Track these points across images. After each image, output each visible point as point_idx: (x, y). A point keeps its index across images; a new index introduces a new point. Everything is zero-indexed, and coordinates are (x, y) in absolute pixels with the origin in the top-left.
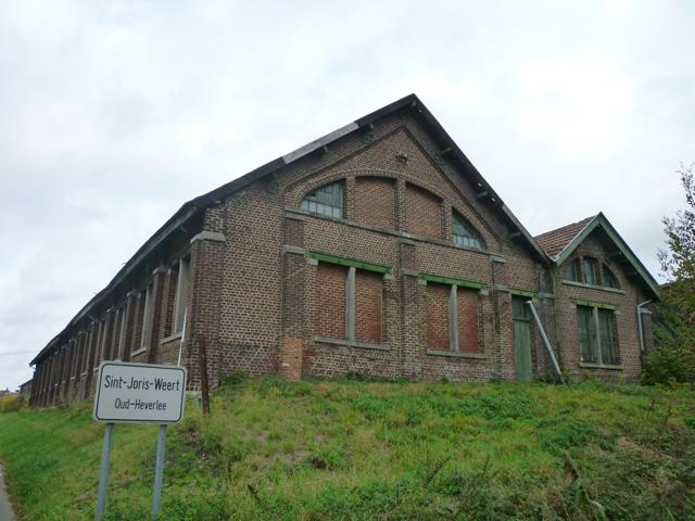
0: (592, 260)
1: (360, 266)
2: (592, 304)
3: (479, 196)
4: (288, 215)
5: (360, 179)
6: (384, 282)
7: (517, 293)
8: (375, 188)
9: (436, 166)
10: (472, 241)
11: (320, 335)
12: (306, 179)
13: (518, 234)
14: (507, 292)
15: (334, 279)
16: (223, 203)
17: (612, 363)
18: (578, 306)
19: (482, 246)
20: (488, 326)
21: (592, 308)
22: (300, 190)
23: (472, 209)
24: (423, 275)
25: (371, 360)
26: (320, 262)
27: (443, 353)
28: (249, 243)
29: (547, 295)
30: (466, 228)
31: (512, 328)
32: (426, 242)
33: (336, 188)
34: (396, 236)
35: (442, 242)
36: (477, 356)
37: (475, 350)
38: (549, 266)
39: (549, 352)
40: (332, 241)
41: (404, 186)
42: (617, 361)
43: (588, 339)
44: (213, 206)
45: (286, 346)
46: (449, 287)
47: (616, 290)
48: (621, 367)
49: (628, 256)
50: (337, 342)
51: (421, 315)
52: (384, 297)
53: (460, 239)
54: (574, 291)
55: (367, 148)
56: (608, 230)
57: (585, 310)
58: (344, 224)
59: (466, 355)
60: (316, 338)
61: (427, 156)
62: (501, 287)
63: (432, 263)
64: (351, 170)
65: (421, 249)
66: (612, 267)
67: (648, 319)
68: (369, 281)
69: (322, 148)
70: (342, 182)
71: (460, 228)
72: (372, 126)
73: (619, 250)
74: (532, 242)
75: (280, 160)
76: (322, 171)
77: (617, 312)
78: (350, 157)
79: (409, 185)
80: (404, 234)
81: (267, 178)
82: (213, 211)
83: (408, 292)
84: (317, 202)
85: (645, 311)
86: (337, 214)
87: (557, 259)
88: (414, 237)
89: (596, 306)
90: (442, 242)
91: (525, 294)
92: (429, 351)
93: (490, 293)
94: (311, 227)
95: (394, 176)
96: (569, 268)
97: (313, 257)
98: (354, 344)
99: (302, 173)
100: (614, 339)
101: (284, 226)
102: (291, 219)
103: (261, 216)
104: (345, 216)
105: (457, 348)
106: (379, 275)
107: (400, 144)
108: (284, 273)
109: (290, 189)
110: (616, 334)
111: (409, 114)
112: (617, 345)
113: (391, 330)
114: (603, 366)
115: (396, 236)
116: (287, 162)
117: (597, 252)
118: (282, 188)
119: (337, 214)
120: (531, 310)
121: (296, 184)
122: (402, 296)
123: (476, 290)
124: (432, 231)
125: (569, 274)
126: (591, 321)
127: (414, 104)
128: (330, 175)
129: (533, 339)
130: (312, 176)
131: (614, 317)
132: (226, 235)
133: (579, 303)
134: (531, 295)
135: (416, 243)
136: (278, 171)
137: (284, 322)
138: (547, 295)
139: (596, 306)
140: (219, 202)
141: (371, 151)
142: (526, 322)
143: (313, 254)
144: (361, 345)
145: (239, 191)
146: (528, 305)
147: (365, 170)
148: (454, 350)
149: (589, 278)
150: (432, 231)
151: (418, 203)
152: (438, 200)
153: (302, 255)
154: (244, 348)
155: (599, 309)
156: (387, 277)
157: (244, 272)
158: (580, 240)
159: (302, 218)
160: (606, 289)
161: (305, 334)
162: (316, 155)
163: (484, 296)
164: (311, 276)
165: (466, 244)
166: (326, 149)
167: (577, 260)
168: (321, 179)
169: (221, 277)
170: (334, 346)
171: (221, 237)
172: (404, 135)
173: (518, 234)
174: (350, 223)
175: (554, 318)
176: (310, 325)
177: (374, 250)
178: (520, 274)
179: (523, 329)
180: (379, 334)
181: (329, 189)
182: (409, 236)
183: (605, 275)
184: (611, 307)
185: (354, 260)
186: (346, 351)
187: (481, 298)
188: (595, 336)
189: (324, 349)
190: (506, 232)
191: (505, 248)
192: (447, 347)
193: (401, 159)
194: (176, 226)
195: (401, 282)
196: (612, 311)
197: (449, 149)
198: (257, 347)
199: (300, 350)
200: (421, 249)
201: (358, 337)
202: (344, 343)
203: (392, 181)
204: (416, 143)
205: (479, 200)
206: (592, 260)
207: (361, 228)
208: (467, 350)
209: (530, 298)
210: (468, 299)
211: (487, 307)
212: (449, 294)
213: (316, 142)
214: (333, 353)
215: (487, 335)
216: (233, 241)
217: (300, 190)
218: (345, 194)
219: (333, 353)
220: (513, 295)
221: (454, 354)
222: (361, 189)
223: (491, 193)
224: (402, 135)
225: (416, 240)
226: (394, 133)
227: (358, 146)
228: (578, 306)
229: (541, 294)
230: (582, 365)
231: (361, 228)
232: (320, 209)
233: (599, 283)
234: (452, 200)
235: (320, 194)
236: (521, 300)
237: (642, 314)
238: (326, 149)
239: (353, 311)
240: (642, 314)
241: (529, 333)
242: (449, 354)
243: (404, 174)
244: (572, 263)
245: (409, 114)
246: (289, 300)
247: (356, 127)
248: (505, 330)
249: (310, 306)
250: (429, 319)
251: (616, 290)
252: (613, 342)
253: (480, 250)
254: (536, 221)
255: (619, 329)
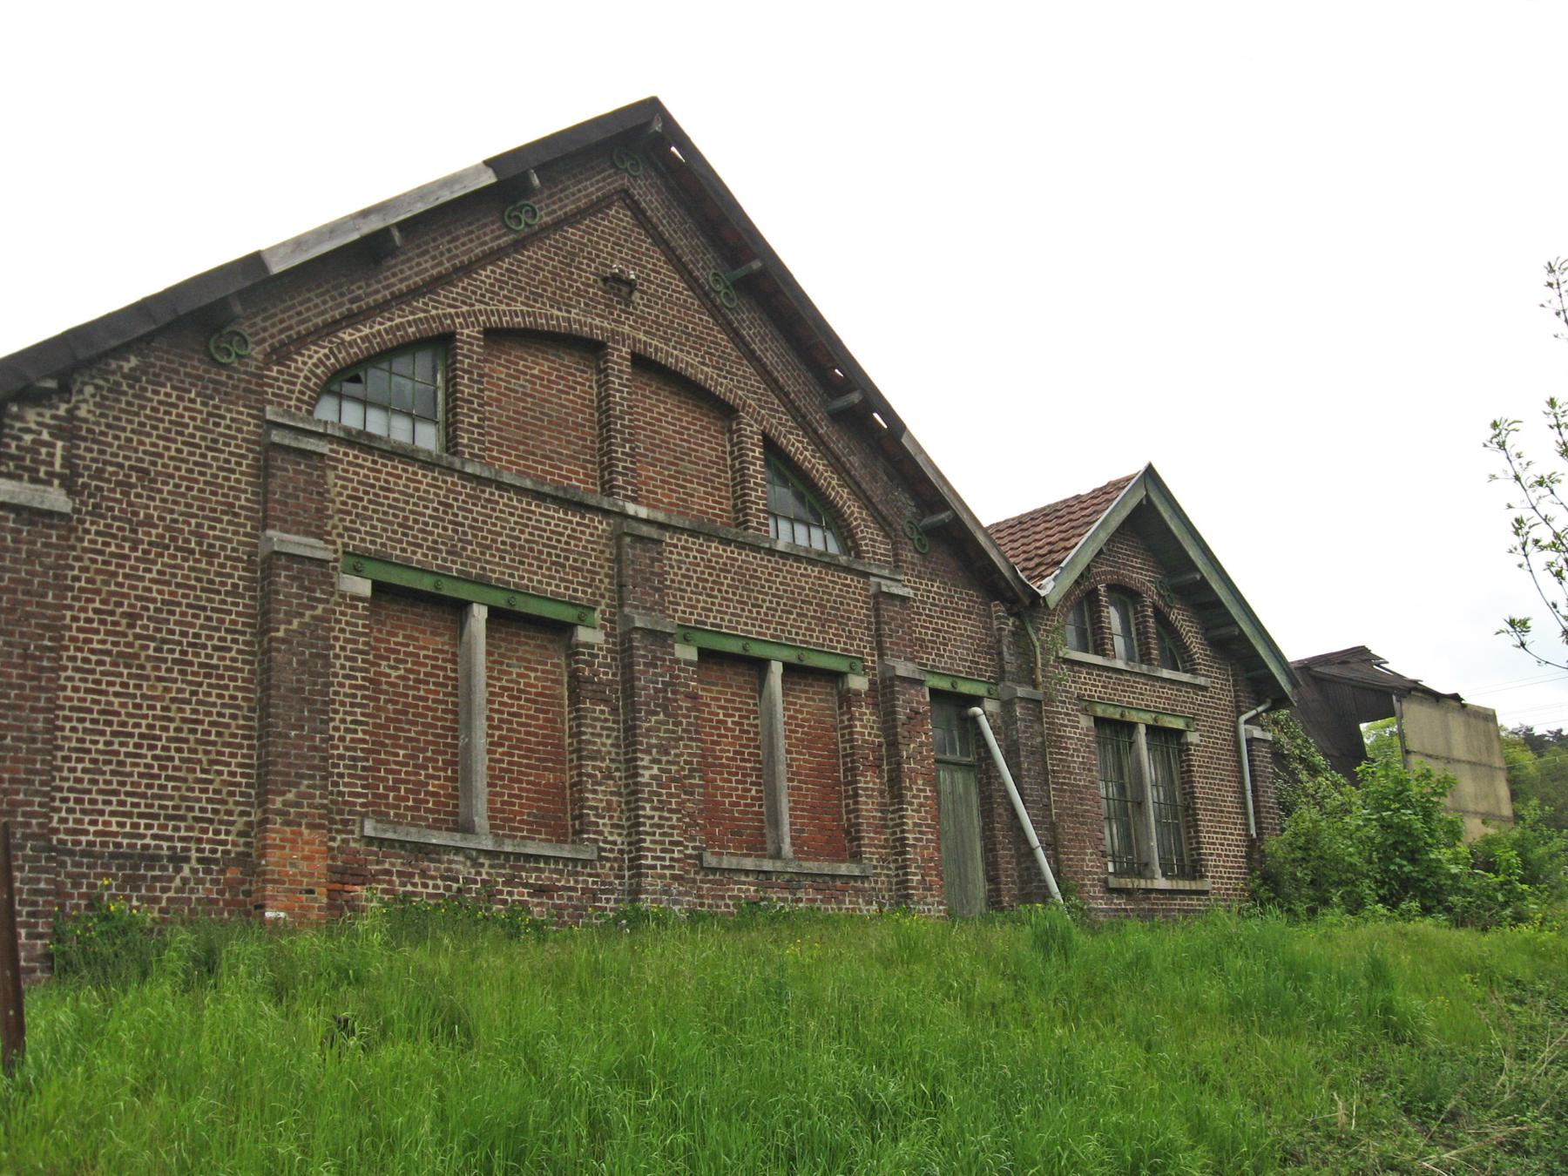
0: (1125, 595)
1: (500, 600)
2: (1132, 716)
3: (840, 403)
4: (276, 437)
5: (496, 336)
6: (572, 651)
7: (944, 684)
8: (538, 366)
9: (715, 311)
10: (817, 534)
11: (381, 817)
12: (334, 326)
13: (944, 516)
14: (921, 683)
15: (419, 643)
16: (64, 390)
17: (1182, 875)
18: (1100, 722)
19: (846, 550)
20: (869, 782)
21: (1131, 727)
22: (312, 360)
23: (819, 443)
24: (687, 633)
25: (540, 891)
26: (378, 587)
27: (749, 863)
28: (148, 522)
29: (1021, 691)
30: (800, 497)
31: (934, 783)
32: (694, 533)
33: (423, 362)
34: (607, 513)
35: (736, 530)
36: (843, 869)
37: (837, 856)
38: (1027, 606)
39: (1032, 851)
40: (420, 526)
41: (626, 366)
42: (1194, 870)
43: (1129, 805)
44: (36, 398)
45: (274, 856)
46: (760, 666)
47: (1186, 677)
48: (1207, 884)
49: (1216, 586)
50: (436, 838)
51: (686, 751)
52: (575, 699)
53: (784, 526)
54: (1096, 675)
55: (519, 245)
56: (1166, 514)
57: (1115, 730)
58: (450, 470)
59: (811, 866)
60: (370, 829)
61: (693, 283)
62: (903, 669)
63: (703, 592)
64: (466, 309)
65: (681, 553)
66: (1177, 616)
67: (1263, 753)
68: (528, 647)
69: (385, 232)
70: (442, 343)
71: (784, 496)
72: (536, 181)
73: (1197, 569)
74: (981, 539)
75: (254, 262)
76: (382, 307)
77: (1193, 737)
78: (467, 269)
79: (642, 363)
80: (631, 508)
81: (202, 323)
82: (31, 416)
83: (647, 683)
84: (365, 403)
85: (1257, 733)
86: (428, 438)
87: (1048, 588)
88: (660, 516)
89: (1142, 719)
90: (736, 530)
91: (965, 688)
92: (710, 860)
93: (872, 683)
94: (348, 476)
95: (598, 335)
96: (1071, 615)
97: (357, 571)
98: (488, 844)
99: (320, 307)
100: (1187, 808)
101: (263, 471)
102: (288, 449)
103: (185, 434)
104: (451, 443)
105: (787, 848)
106: (560, 630)
107: (613, 243)
108: (263, 621)
109: (281, 354)
110: (1190, 795)
111: (638, 155)
112: (1193, 825)
113: (599, 796)
114: (1161, 883)
115: (607, 513)
116: (276, 268)
117: (1141, 575)
118: (256, 352)
119: (428, 438)
120: (980, 734)
121: (302, 341)
122: (629, 691)
123: (836, 677)
124: (708, 502)
125: (1071, 633)
126: (1128, 764)
127: (658, 127)
128: (406, 321)
129: (987, 814)
130: (351, 319)
131: (1184, 748)
132: (71, 491)
133: (1100, 711)
134: (980, 690)
135: (667, 537)
136: (245, 295)
137: (263, 783)
138: (1021, 691)
139: (1142, 719)
140: (51, 384)
141: (531, 254)
142: (968, 767)
143: (357, 561)
144: (508, 847)
145: (120, 352)
146: (975, 718)
147: (515, 311)
148: (777, 855)
149: (1119, 643)
150: (708, 502)
151: (663, 414)
152: (724, 411)
153: (322, 563)
154: (136, 866)
155: (1148, 727)
156: (583, 635)
157: (132, 617)
158: (1104, 536)
159: (324, 448)
160: (1166, 673)
161: (333, 818)
162: (365, 254)
163: (857, 693)
164: (349, 630)
165: (818, 545)
166: (396, 235)
167: (1092, 594)
168: (377, 329)
169: (55, 628)
170: (424, 851)
171: (56, 499)
172: (626, 218)
173: (944, 516)
174: (469, 469)
175: (1040, 754)
176: (349, 787)
177: (549, 555)
178: (947, 636)
179: (960, 789)
180: (563, 815)
181: (401, 364)
182: (643, 512)
183: (1160, 637)
184: (1178, 724)
185: (482, 582)
186: (463, 869)
187: (847, 699)
188: (1140, 804)
189: (397, 864)
190: (910, 509)
191: (908, 555)
192: (756, 846)
193: (618, 286)
194: (1215, 587)
195: (623, 649)
196: (1179, 733)
197: (756, 265)
198: (178, 859)
199: (320, 865)
200: (681, 553)
201: (501, 822)
202: (456, 840)
203: (591, 349)
204: (660, 241)
205: (837, 417)
206: (1125, 595)
207: (501, 486)
208: (814, 855)
209: (977, 700)
210: (813, 701)
211: (866, 724)
212: (1492, 779)
213: (365, 214)
214: (423, 874)
215: (869, 808)
216: (96, 513)
217: (312, 360)
218: (451, 382)
219: (423, 874)
220: (935, 692)
221: (779, 865)
222: (499, 369)
223: (873, 400)
224: (619, 216)
225: (663, 526)
226: (597, 207)
227: (490, 236)
228: (1100, 722)
229: (1005, 688)
230: (1114, 882)
231: (501, 486)
232: (376, 423)
233: (1145, 658)
234: (762, 415)
235: (375, 378)
236: (954, 704)
237: (1250, 741)
238: (396, 235)
239: (481, 741)
240: (1250, 741)
241: (975, 800)
242: (768, 865)
243: (627, 331)
244: (1079, 603)
245: (638, 155)
246: (279, 702)
247: (489, 178)
248: (917, 792)
249: (347, 726)
250: (707, 764)
251: (1186, 677)
252: (1183, 815)
253: (843, 559)
254: (994, 485)
255: (1199, 781)
